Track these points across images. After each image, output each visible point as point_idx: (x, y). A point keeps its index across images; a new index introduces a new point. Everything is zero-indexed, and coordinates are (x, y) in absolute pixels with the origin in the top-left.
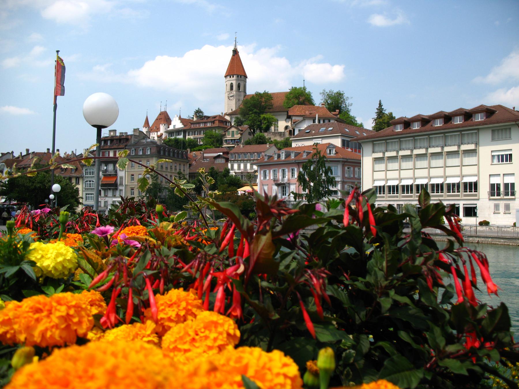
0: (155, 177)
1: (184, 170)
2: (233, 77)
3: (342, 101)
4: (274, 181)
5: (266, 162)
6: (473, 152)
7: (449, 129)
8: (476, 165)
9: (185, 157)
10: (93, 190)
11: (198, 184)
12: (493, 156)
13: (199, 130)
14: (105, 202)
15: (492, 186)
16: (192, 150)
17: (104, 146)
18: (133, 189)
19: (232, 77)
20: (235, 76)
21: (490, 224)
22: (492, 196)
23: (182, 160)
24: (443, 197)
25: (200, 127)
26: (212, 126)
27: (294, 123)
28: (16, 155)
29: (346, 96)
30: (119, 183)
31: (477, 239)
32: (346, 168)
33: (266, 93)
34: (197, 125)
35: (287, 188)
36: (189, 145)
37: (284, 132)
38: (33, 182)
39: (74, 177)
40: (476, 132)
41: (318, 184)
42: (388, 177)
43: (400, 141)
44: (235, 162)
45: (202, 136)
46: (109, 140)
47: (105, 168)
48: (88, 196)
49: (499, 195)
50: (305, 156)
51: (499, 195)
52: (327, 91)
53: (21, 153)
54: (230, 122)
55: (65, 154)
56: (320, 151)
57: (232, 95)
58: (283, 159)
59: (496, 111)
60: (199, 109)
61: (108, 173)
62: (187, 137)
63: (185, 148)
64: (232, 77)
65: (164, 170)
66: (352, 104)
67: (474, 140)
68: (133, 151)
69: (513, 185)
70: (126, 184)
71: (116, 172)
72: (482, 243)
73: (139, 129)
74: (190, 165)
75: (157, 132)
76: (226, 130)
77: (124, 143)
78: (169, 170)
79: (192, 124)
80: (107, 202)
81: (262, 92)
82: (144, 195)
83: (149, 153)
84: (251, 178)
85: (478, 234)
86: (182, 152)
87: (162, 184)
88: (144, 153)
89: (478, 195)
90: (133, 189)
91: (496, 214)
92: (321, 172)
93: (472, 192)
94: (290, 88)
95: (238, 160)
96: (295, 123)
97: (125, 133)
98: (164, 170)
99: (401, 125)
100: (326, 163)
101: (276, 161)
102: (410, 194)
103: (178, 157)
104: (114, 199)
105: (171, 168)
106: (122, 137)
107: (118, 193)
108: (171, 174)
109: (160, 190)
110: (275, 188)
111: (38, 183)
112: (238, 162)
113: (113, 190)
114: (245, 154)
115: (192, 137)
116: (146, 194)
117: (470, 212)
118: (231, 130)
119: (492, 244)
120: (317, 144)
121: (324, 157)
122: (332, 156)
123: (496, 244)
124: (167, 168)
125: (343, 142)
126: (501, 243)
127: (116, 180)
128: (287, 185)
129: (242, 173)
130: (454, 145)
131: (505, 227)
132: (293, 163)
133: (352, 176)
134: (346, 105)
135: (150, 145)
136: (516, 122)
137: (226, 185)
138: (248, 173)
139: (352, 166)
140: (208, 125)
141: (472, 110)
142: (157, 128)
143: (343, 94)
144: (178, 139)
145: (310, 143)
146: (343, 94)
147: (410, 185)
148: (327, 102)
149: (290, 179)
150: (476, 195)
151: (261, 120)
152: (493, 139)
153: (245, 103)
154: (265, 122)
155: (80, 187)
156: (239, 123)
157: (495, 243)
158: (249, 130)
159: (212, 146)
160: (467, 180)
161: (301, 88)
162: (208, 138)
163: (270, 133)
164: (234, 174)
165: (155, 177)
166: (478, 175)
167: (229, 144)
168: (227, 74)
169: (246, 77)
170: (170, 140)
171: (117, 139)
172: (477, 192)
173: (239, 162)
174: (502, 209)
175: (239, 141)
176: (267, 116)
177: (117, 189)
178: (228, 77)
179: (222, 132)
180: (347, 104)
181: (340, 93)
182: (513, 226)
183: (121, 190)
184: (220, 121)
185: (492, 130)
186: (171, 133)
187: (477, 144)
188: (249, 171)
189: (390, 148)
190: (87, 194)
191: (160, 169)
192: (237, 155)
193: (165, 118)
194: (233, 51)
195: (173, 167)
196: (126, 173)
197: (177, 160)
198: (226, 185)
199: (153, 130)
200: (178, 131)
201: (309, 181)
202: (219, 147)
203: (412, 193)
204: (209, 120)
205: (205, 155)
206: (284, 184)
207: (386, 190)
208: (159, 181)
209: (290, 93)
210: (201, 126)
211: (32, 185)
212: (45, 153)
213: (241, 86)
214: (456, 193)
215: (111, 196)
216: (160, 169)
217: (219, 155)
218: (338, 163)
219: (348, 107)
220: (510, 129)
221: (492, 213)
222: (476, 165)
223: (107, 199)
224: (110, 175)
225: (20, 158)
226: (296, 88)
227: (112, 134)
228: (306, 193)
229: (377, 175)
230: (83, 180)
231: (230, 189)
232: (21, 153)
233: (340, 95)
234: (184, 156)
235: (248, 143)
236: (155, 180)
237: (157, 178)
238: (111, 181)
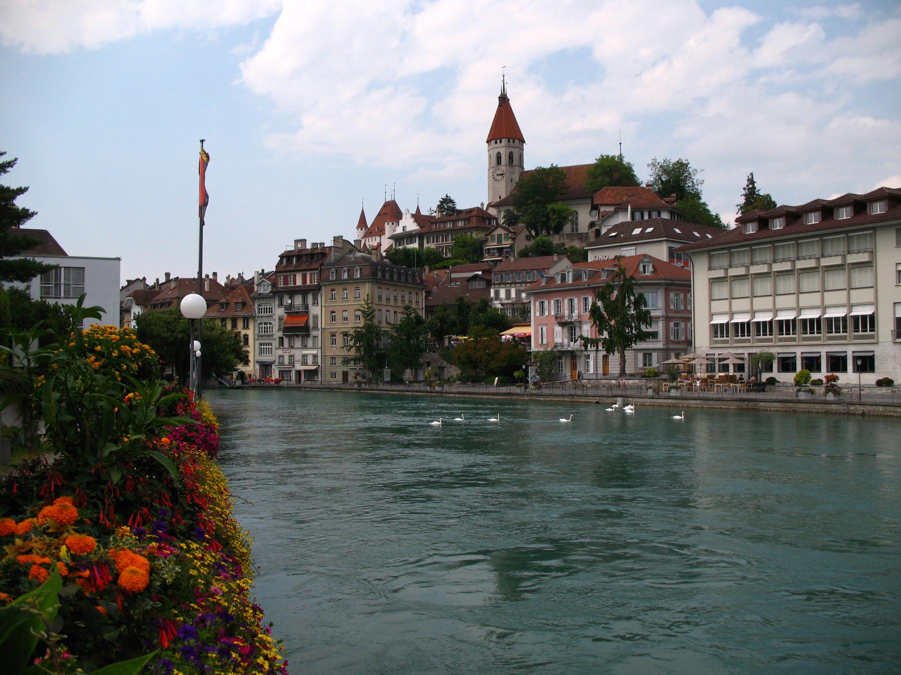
0: (369, 315)
2: (501, 142)
4: (556, 318)
7: (828, 228)
8: (873, 287)
9: (419, 281)
10: (270, 337)
11: (439, 324)
13: (445, 233)
14: (290, 356)
17: (287, 266)
18: (335, 336)
19: (498, 141)
20: (503, 140)
21: (895, 383)
23: (414, 286)
24: (772, 342)
26: (468, 227)
27: (603, 217)
28: (150, 282)
29: (692, 166)
31: (861, 408)
32: (672, 295)
33: (554, 168)
34: (442, 226)
35: (577, 329)
36: (427, 260)
37: (587, 233)
38: (173, 332)
39: (240, 317)
40: (871, 234)
42: (755, 308)
43: (752, 250)
44: (501, 286)
46: (294, 256)
47: (289, 301)
48: (263, 347)
50: (604, 277)
53: (157, 280)
54: (497, 219)
55: (227, 278)
56: (625, 269)
57: (500, 172)
58: (570, 282)
60: (447, 196)
62: (426, 245)
64: (498, 141)
65: (384, 302)
67: (869, 246)
68: (332, 273)
70: (323, 327)
71: (307, 307)
72: (869, 415)
73: (342, 237)
74: (428, 293)
75: (380, 236)
76: (489, 231)
78: (392, 303)
84: (522, 315)
85: (863, 400)
86: (413, 273)
88: (351, 276)
89: (876, 337)
90: (335, 336)
92: (627, 304)
94: (598, 157)
95: (506, 284)
96: (605, 217)
97: (321, 244)
98: (384, 302)
99: (754, 224)
100: (635, 287)
101: (559, 286)
102: (768, 337)
105: (396, 300)
106: (315, 252)
108: (394, 309)
111: (180, 332)
113: (303, 336)
115: (432, 246)
116: (355, 342)
117: (866, 364)
120: (621, 257)
121: (632, 278)
123: (890, 416)
124: (388, 299)
125: (671, 252)
128: (577, 324)
129: (512, 304)
130: (837, 255)
132: (585, 289)
133: (682, 308)
134: (693, 183)
135: (361, 263)
138: (523, 304)
139: (682, 291)
140: (460, 225)
141: (865, 196)
142: (380, 229)
143: (687, 165)
145: (611, 254)
146: (687, 165)
147: (769, 322)
150: (872, 337)
151: (548, 214)
153: (520, 185)
154: (554, 217)
155: (250, 333)
156: (511, 220)
157: (889, 414)
158: (526, 232)
159: (465, 259)
160: (858, 312)
161: (613, 158)
162: (459, 246)
163: (563, 236)
164: (499, 306)
165: (369, 315)
166: (875, 303)
167: (493, 255)
170: (397, 251)
172: (874, 331)
173: (507, 286)
175: (509, 250)
176: (559, 206)
177: (308, 336)
178: (493, 142)
180: (695, 181)
181: (682, 163)
183: (314, 337)
184: (478, 217)
185: (897, 229)
186: (398, 239)
187: (872, 252)
188: (525, 301)
190: (261, 344)
191: (377, 302)
193: (391, 211)
195: (399, 299)
196: (323, 308)
197: (396, 285)
199: (373, 233)
200: (409, 236)
201: (609, 318)
202: (477, 262)
203: (820, 333)
204: (461, 216)
206: (572, 323)
207: (753, 329)
208: (376, 322)
209: (596, 166)
212: (194, 279)
213: (515, 159)
214: (816, 335)
215: (300, 346)
216: (377, 302)
217: (476, 276)
218: (658, 287)
219: (696, 187)
222: (873, 287)
223: (293, 352)
225: (156, 289)
226: (608, 157)
227: (299, 246)
228: (603, 337)
229: (717, 306)
230: (255, 321)
231: (487, 332)
232: (157, 280)
233: (681, 167)
234: (418, 279)
236: (369, 320)
237: (373, 317)
238: (300, 322)
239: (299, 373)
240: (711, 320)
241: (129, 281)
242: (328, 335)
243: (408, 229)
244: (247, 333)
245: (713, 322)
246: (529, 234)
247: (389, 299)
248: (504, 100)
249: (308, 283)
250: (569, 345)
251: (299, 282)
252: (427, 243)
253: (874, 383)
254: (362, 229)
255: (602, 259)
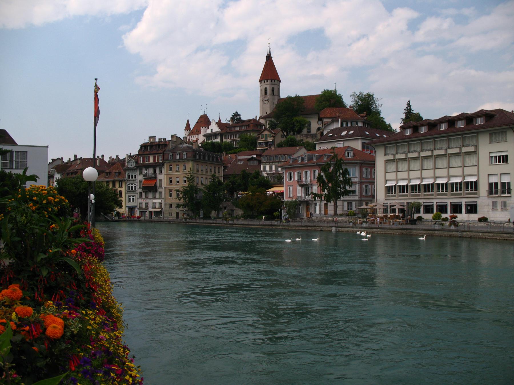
0: (191, 180)
1: (219, 173)
2: (267, 82)
3: (372, 102)
4: (298, 182)
5: (290, 165)
6: (474, 153)
8: (476, 166)
9: (220, 161)
10: (135, 192)
11: (231, 185)
12: (491, 157)
13: (235, 133)
14: (146, 203)
15: (491, 185)
16: (228, 152)
17: (144, 151)
18: (171, 191)
19: (266, 81)
20: (269, 81)
21: (489, 220)
22: (490, 194)
24: (395, 197)
25: (241, 130)
27: (325, 125)
28: (65, 160)
29: (376, 96)
30: (158, 185)
32: (364, 169)
35: (310, 189)
37: (316, 134)
39: (117, 181)
41: (337, 184)
43: (435, 141)
44: (267, 164)
45: (238, 138)
46: (149, 145)
47: (146, 172)
48: (130, 198)
49: (496, 193)
51: (496, 193)
52: (358, 93)
53: (70, 159)
54: (264, 125)
55: (110, 158)
58: (306, 162)
59: (496, 115)
60: (236, 112)
61: (148, 177)
62: (224, 140)
63: (221, 151)
64: (266, 81)
65: (200, 173)
66: (382, 105)
67: (474, 142)
68: (170, 155)
69: (509, 183)
70: (165, 186)
71: (156, 175)
72: (474, 238)
73: (176, 135)
74: (225, 168)
76: (260, 132)
77: (162, 148)
78: (204, 173)
79: (228, 128)
80: (148, 203)
81: (293, 95)
82: (181, 197)
83: (185, 157)
84: (279, 180)
85: (471, 229)
87: (198, 186)
88: (181, 157)
90: (171, 191)
91: (494, 211)
92: (338, 174)
93: (444, 191)
94: (322, 91)
97: (164, 139)
98: (200, 173)
101: (299, 164)
103: (213, 160)
104: (154, 201)
105: (207, 171)
106: (161, 143)
107: (157, 195)
109: (196, 191)
110: (299, 188)
111: (83, 189)
112: (269, 164)
113: (153, 192)
114: (276, 156)
115: (228, 140)
116: (183, 195)
117: (472, 209)
118: (264, 133)
119: (482, 238)
120: (335, 148)
121: (341, 160)
122: (350, 159)
123: (486, 238)
124: (202, 171)
126: (490, 237)
127: (156, 183)
128: (310, 186)
129: (273, 174)
131: (501, 223)
133: (369, 177)
134: (376, 106)
136: (510, 125)
137: (256, 186)
138: (279, 174)
139: (369, 167)
143: (372, 96)
144: (214, 142)
145: (329, 146)
148: (357, 103)
149: (313, 180)
150: (476, 194)
152: (491, 142)
153: (278, 106)
155: (123, 189)
156: (273, 126)
157: (485, 237)
158: (281, 133)
159: (246, 148)
160: (468, 179)
161: (331, 91)
163: (302, 135)
164: (266, 175)
165: (191, 180)
166: (478, 175)
167: (262, 146)
168: (261, 79)
169: (279, 81)
170: (207, 143)
171: (156, 145)
172: (477, 190)
173: (270, 163)
174: (499, 207)
175: (272, 143)
176: (300, 118)
177: (156, 191)
178: (263, 82)
179: (255, 135)
181: (370, 94)
182: (508, 222)
183: (160, 192)
184: (254, 124)
185: (490, 133)
186: (208, 136)
188: (280, 172)
189: (400, 150)
190: (129, 196)
192: (268, 157)
193: (204, 121)
194: (266, 56)
198: (256, 186)
200: (214, 135)
201: (328, 182)
202: (253, 150)
204: (244, 124)
205: (240, 158)
206: (307, 185)
207: (409, 189)
210: (237, 129)
211: (77, 191)
212: (91, 159)
213: (275, 91)
214: (444, 192)
217: (253, 158)
218: (356, 165)
219: (378, 108)
220: (506, 132)
221: (491, 210)
222: (476, 166)
223: (148, 201)
224: (150, 178)
225: (69, 164)
226: (328, 90)
227: (152, 140)
228: (325, 193)
229: (389, 176)
230: (126, 183)
232: (70, 159)
234: (219, 159)
235: (280, 146)
236: (191, 183)
237: (194, 181)
239: (151, 213)
240: (386, 183)
241: (53, 160)
242: (168, 191)
243: (214, 131)
244: (121, 190)
245: (387, 185)
246: (283, 134)
247: (203, 171)
248: (269, 58)
249: (157, 161)
250: (305, 198)
251: (151, 161)
252: (225, 139)
253: (477, 219)
254: (187, 131)
255: (324, 149)
